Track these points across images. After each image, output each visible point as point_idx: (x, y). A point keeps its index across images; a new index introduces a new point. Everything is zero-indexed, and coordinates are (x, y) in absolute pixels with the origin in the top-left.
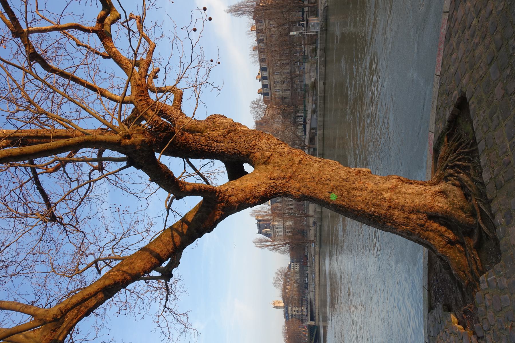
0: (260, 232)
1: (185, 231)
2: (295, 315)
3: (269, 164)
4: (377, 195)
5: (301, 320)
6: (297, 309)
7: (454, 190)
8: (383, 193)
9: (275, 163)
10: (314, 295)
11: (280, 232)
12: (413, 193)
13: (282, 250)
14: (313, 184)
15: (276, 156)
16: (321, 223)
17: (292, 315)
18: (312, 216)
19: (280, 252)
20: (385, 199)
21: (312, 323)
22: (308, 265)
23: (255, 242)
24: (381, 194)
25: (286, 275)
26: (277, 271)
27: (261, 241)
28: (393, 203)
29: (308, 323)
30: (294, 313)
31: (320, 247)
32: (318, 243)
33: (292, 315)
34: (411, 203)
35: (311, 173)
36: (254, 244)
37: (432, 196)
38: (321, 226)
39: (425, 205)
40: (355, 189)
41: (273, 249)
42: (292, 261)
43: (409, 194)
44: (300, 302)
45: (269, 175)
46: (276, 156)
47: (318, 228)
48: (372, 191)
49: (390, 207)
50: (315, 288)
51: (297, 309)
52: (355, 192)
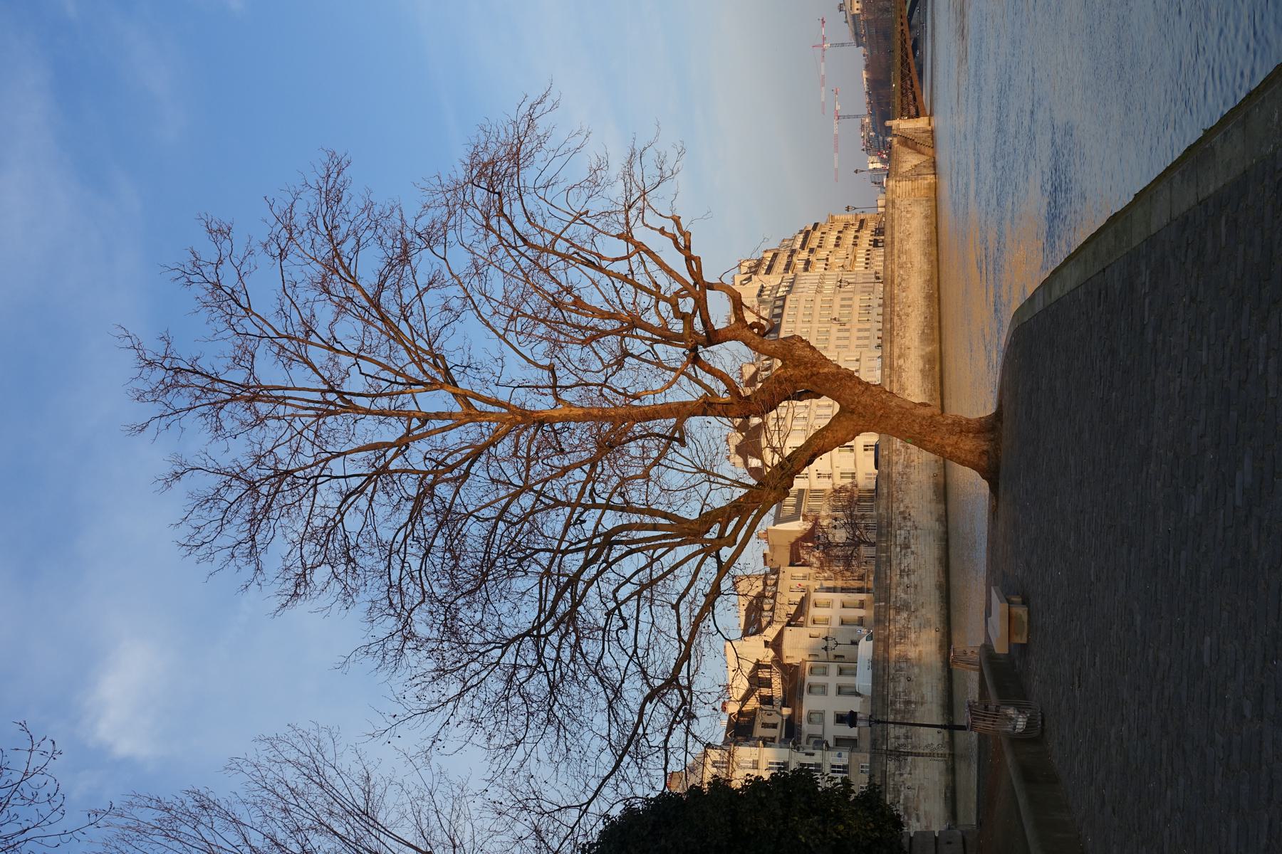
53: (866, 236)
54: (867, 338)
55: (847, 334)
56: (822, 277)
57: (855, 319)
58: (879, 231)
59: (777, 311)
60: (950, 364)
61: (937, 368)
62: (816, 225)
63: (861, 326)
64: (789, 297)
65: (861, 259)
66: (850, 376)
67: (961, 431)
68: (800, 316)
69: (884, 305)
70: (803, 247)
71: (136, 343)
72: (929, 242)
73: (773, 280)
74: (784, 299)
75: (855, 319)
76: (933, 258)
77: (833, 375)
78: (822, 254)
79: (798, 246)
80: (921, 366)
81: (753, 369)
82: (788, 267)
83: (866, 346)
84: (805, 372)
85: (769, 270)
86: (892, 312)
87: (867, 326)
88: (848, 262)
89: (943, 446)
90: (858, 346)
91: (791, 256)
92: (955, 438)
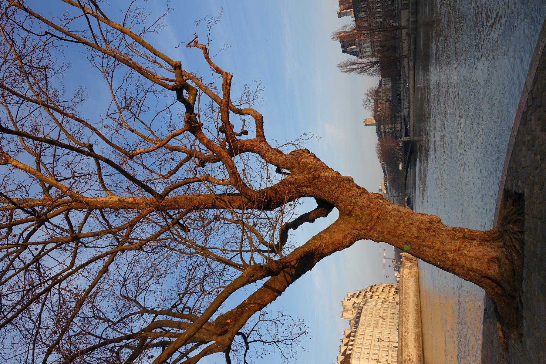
0: (344, 51)
1: (293, 273)
2: (389, 132)
3: (351, 215)
4: (443, 254)
5: (395, 135)
6: (390, 126)
7: (506, 264)
8: (448, 253)
9: (357, 216)
10: (409, 112)
11: (369, 51)
12: (473, 257)
13: (371, 71)
14: (390, 236)
15: (357, 209)
16: (416, 34)
17: (385, 133)
18: (404, 28)
19: (368, 74)
20: (449, 258)
21: (407, 139)
22: (402, 82)
23: (340, 66)
24: (446, 254)
25: (377, 94)
26: (366, 92)
27: (347, 64)
28: (455, 262)
29: (402, 139)
30: (388, 130)
31: (415, 62)
32: (412, 58)
33: (385, 133)
34: (470, 265)
35: (387, 228)
36: (339, 69)
37: (488, 263)
38: (415, 38)
39: (480, 271)
40: (424, 246)
41: (361, 72)
42: (383, 76)
43: (469, 257)
44: (393, 119)
45: (352, 227)
46: (357, 209)
47: (412, 41)
48: (439, 250)
49: (453, 265)
50: (409, 105)
51: (390, 126)
52: (425, 248)
53: (393, 290)
54: (393, 325)
55: (385, 323)
56: (377, 301)
57: (389, 318)
58: (398, 289)
59: (359, 311)
60: (427, 337)
61: (421, 338)
62: (375, 285)
63: (391, 321)
64: (364, 307)
65: (391, 297)
66: (350, 180)
67: (464, 237)
68: (368, 314)
69: (399, 311)
70: (370, 291)
71: (116, 271)
72: (416, 291)
73: (358, 301)
74: (362, 307)
75: (389, 318)
76: (418, 297)
77: (333, 178)
78: (377, 294)
79: (368, 290)
80: (414, 336)
81: (349, 332)
82: (364, 297)
83: (392, 328)
84: (308, 176)
85: (358, 297)
86: (402, 314)
87: (393, 321)
88: (386, 297)
89: (444, 252)
90: (389, 328)
91: (366, 293)
92: (458, 243)
